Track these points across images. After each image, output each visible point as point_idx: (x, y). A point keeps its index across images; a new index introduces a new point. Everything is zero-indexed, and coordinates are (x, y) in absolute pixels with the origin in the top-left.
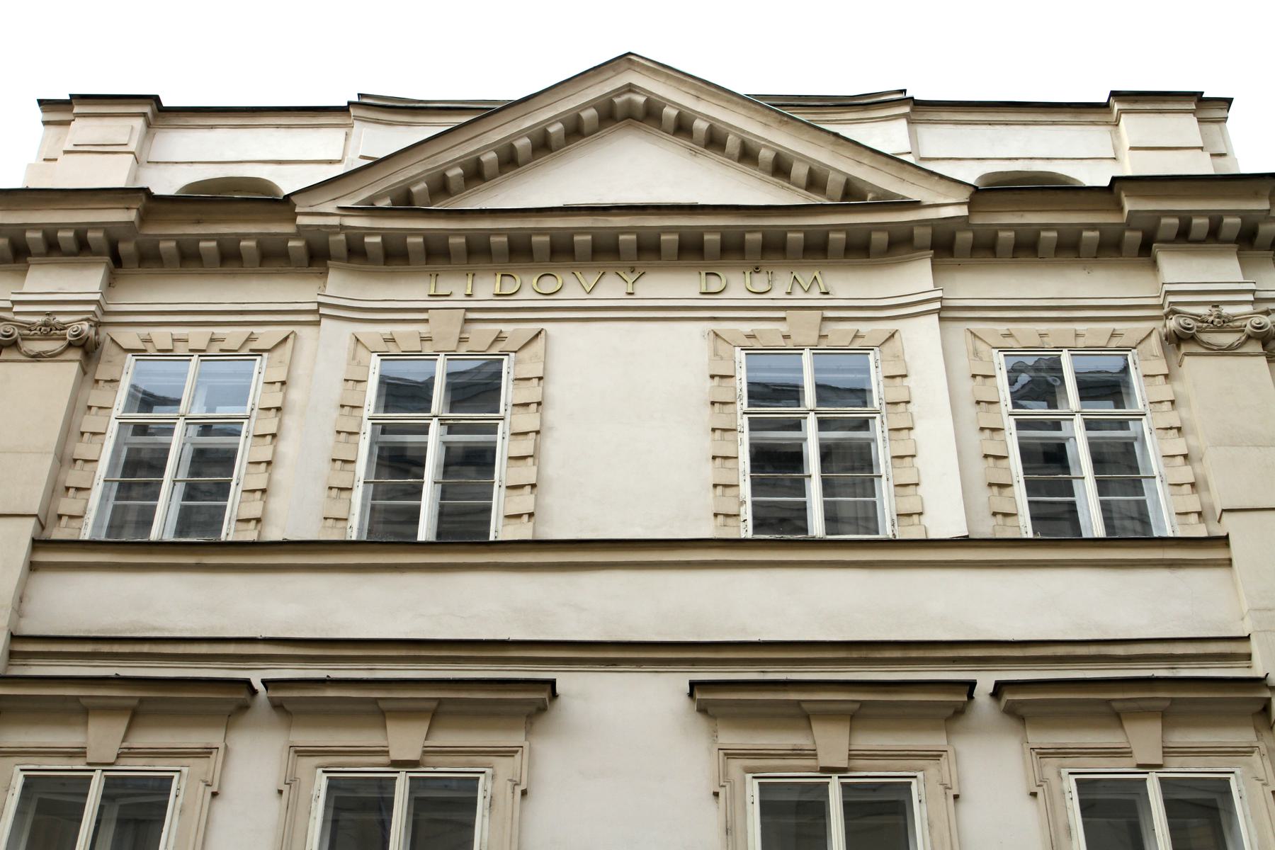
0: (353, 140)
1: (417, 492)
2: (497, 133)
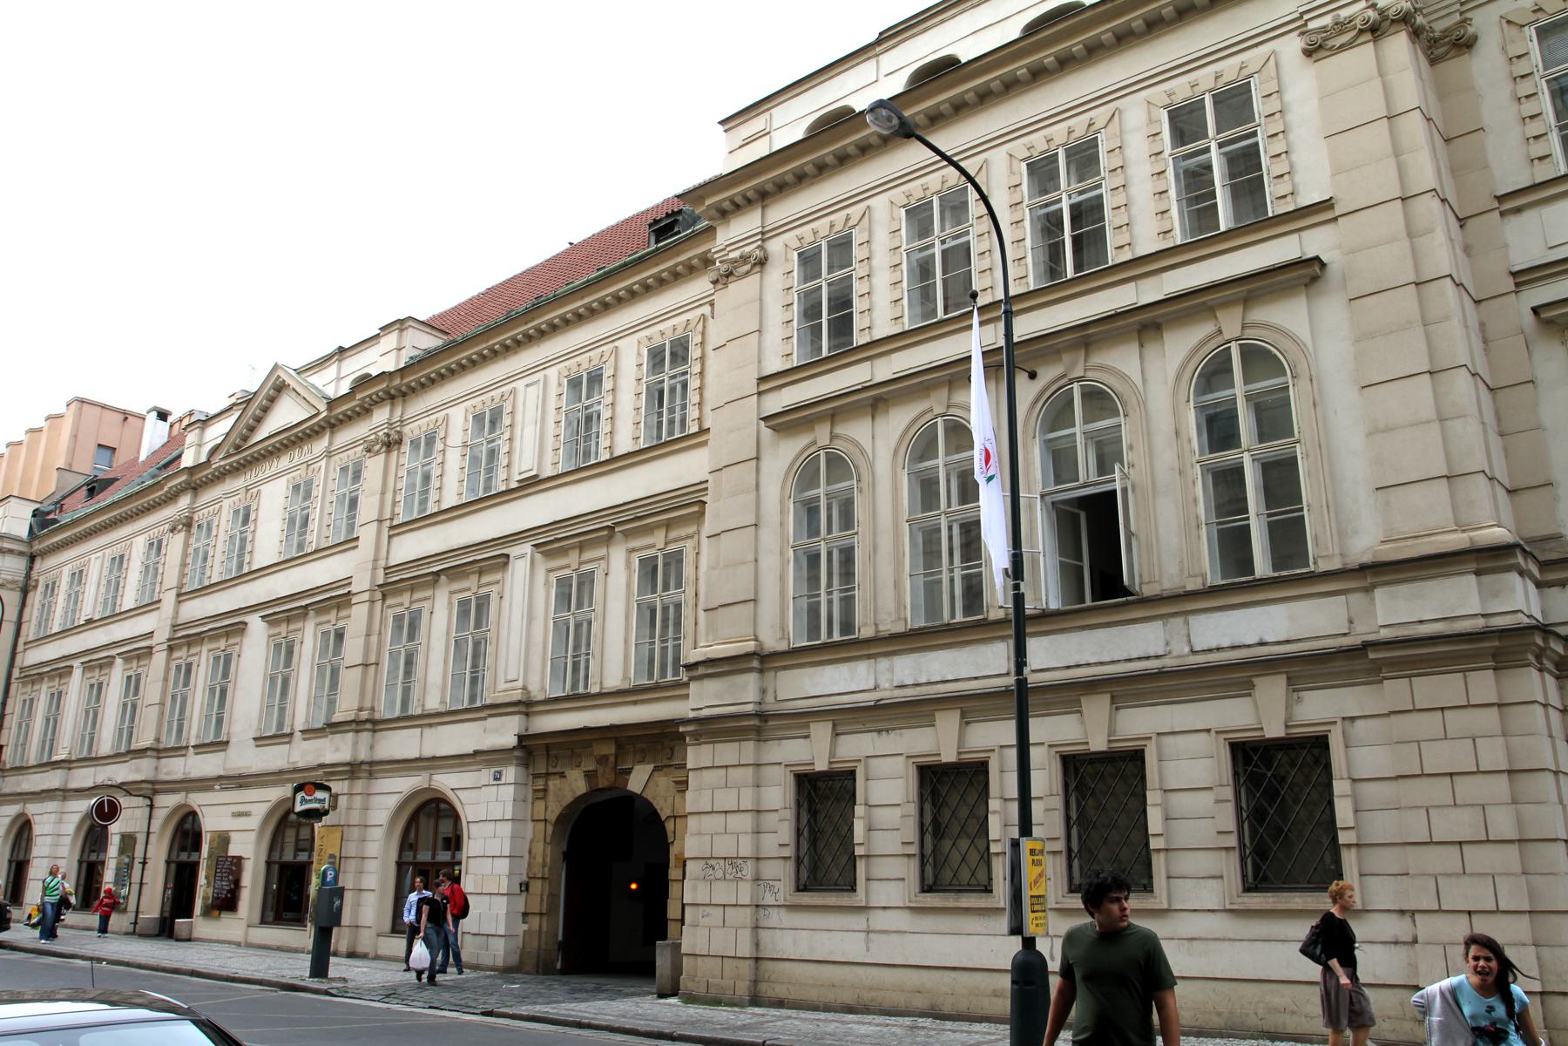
0: (881, 64)
1: (1213, 195)
2: (255, 404)
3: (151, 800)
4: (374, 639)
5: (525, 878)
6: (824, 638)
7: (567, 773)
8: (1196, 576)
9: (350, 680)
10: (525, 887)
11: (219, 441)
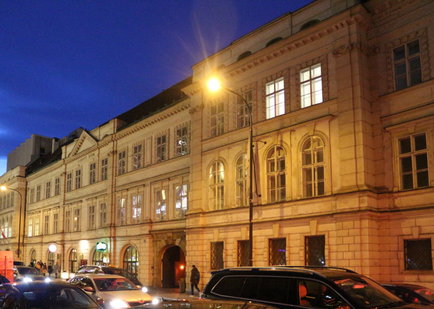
3: (64, 245)
4: (113, 206)
5: (152, 266)
6: (276, 200)
7: (161, 240)
8: (299, 196)
9: (108, 216)
10: (153, 268)
11: (71, 151)
